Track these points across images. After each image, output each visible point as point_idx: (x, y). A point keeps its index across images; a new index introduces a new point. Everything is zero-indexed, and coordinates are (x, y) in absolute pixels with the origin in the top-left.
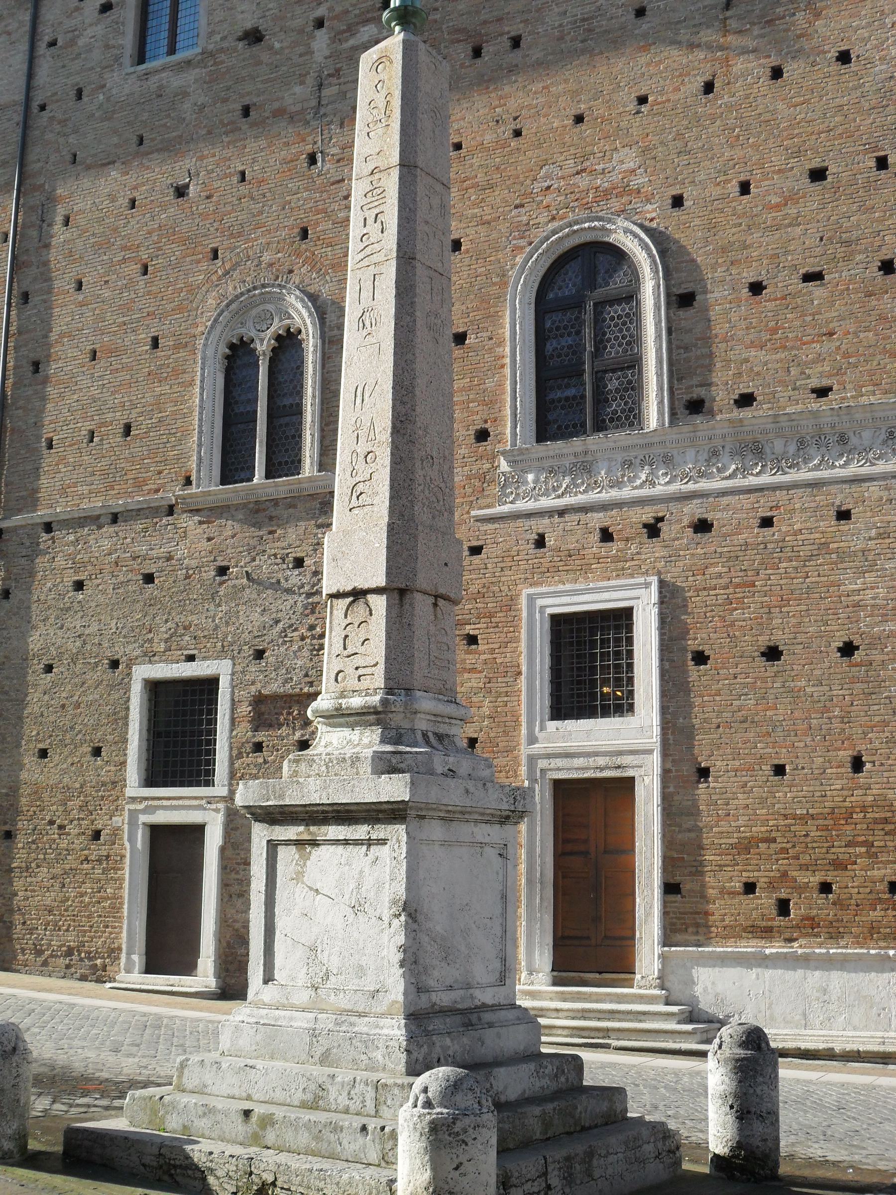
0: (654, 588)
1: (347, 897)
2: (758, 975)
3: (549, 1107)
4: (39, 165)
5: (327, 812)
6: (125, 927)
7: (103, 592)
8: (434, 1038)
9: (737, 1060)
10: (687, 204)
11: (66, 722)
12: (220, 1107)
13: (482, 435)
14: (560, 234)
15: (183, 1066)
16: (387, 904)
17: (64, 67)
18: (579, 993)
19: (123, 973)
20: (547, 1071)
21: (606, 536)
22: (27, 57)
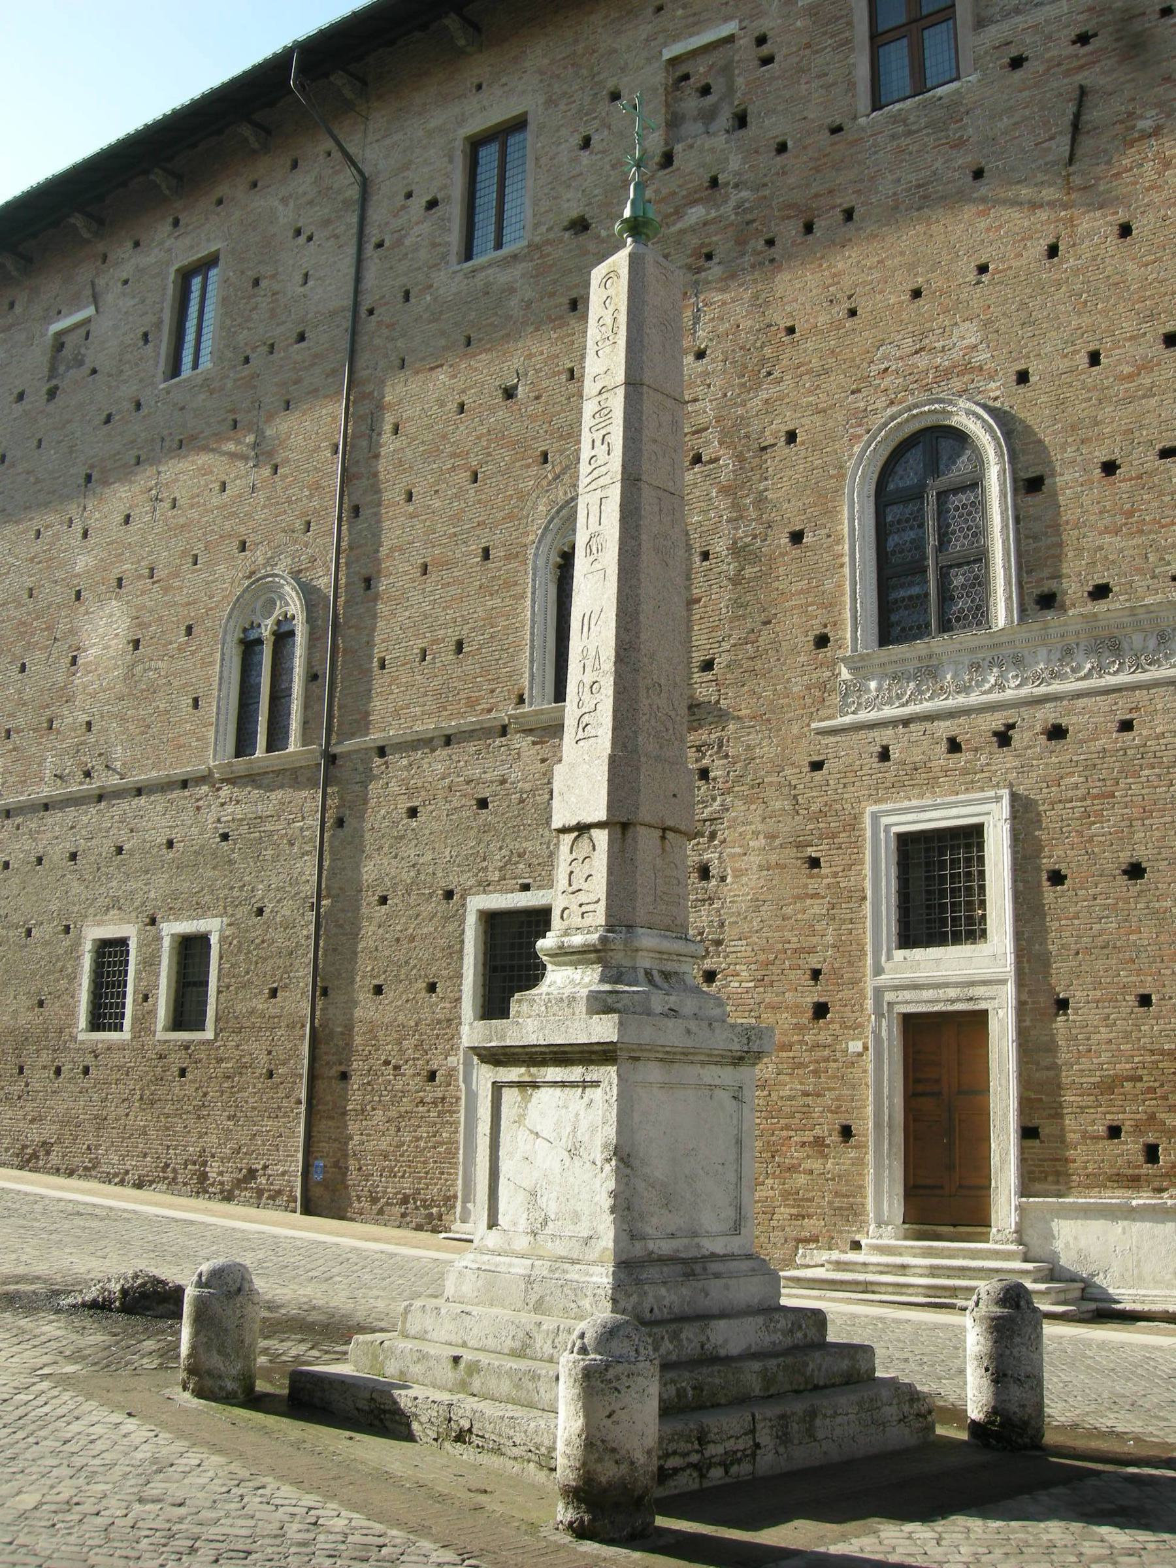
0: (1006, 801)
1: (564, 1140)
2: (1124, 1228)
3: (772, 1363)
4: (368, 371)
5: (545, 1053)
6: (461, 1173)
7: (437, 818)
8: (646, 1287)
9: (993, 1319)
10: (1032, 379)
11: (400, 956)
12: (432, 1352)
13: (822, 641)
14: (899, 420)
15: (407, 1311)
16: (599, 1149)
17: (391, 268)
18: (930, 1248)
19: (458, 1223)
20: (779, 1326)
21: (954, 746)
22: (354, 261)
